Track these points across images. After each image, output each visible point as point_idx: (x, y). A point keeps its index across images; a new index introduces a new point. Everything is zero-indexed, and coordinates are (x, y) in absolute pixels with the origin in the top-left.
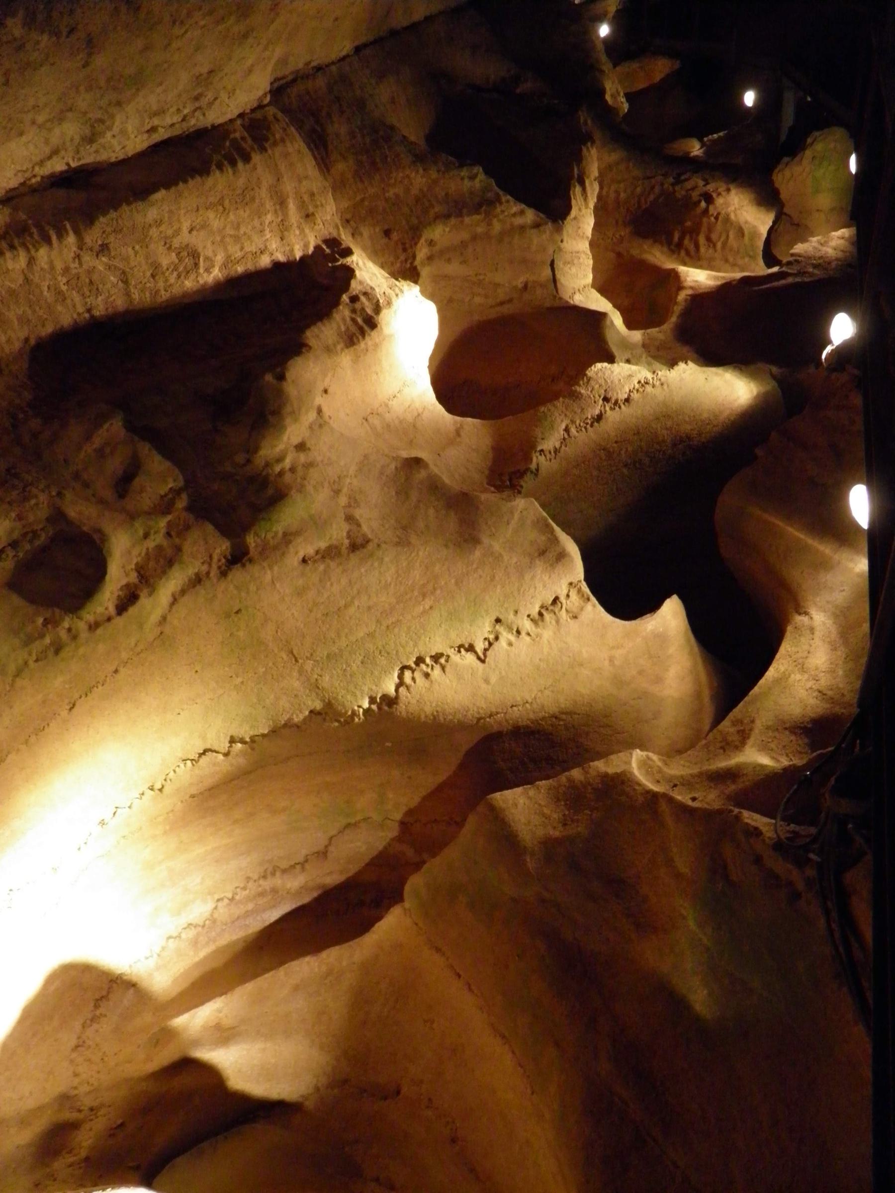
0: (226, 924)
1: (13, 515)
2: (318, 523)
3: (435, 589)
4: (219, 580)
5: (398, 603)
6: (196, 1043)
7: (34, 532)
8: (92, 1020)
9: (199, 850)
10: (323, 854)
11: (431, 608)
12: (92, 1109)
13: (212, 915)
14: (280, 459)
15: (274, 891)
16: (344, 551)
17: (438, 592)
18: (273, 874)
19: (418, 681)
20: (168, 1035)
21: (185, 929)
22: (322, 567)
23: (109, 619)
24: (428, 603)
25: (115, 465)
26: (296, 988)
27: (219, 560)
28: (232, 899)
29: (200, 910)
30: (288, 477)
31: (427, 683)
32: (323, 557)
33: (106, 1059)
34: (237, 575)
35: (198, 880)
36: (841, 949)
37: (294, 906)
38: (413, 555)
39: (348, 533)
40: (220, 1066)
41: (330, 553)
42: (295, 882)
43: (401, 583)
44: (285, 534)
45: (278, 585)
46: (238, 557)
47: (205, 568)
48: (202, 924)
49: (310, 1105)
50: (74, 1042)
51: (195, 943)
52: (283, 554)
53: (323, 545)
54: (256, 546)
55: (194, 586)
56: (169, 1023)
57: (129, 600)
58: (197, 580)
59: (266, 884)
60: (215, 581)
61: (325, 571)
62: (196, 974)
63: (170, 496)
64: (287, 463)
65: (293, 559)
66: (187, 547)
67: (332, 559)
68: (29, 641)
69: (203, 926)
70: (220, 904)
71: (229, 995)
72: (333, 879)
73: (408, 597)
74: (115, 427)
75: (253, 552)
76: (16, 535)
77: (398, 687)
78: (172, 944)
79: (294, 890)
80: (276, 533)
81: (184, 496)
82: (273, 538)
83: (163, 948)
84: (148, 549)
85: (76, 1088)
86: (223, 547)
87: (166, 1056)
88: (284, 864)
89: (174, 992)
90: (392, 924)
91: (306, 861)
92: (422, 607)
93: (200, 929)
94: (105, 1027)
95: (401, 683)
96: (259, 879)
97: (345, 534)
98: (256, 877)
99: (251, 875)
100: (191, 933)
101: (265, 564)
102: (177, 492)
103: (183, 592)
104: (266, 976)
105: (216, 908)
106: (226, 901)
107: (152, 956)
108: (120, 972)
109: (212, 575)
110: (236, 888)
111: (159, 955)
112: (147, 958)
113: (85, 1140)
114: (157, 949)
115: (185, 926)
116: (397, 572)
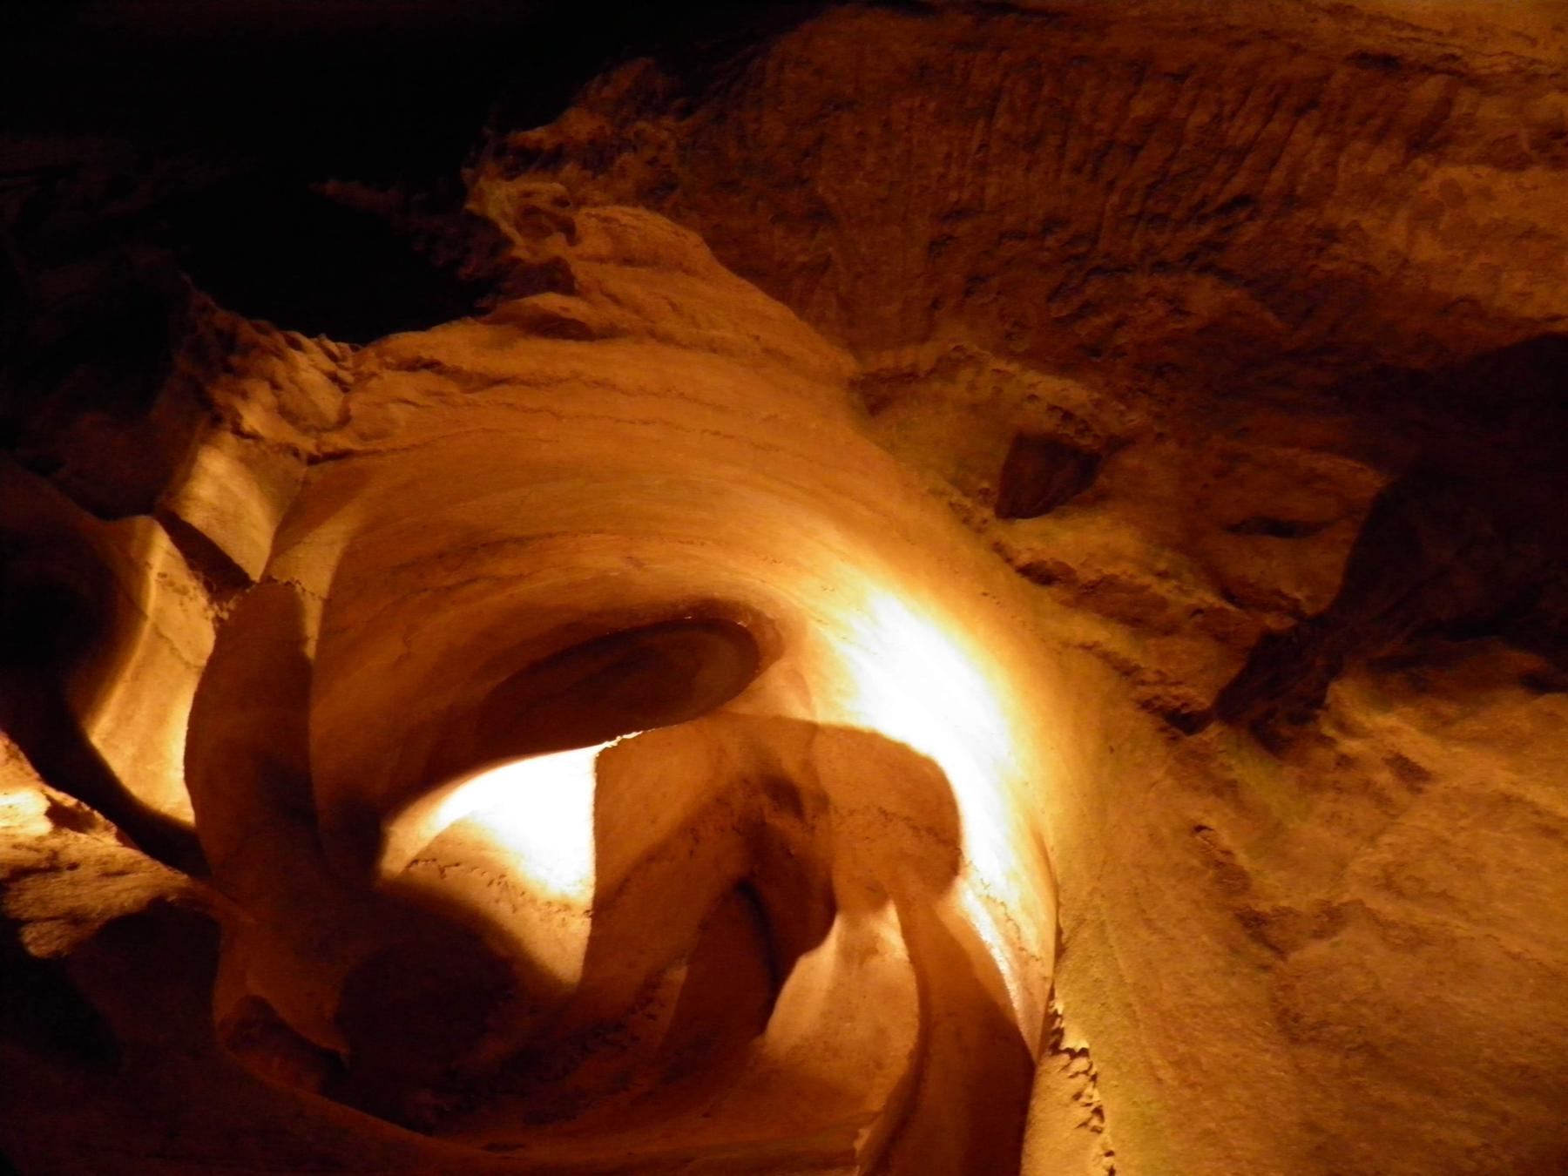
1: (1096, 396)
2: (1272, 838)
3: (1192, 1086)
4: (1138, 701)
5: (1162, 1013)
7: (1088, 429)
8: (915, 828)
11: (1159, 1081)
12: (813, 828)
14: (1346, 728)
16: (1239, 901)
17: (1187, 1093)
19: (1073, 1081)
20: (876, 899)
22: (1195, 863)
23: (1009, 560)
24: (1167, 1074)
25: (1301, 505)
27: (1177, 698)
30: (1320, 754)
31: (1067, 1098)
32: (1219, 864)
34: (1145, 725)
38: (1259, 1040)
39: (1288, 912)
41: (1228, 877)
43: (1195, 1016)
44: (1233, 785)
45: (1151, 795)
46: (1179, 722)
47: (1150, 676)
49: (757, 1041)
50: (890, 809)
52: (1197, 789)
53: (1243, 859)
54: (1206, 744)
55: (1116, 668)
57: (1041, 576)
58: (1126, 671)
60: (1133, 695)
61: (1192, 868)
63: (1284, 603)
64: (1351, 746)
65: (1198, 808)
66: (1179, 645)
67: (1218, 881)
68: (959, 483)
73: (1173, 1032)
74: (1368, 481)
75: (1193, 740)
76: (1079, 413)
77: (1070, 1051)
80: (1230, 768)
81: (1289, 622)
82: (1222, 765)
84: (1149, 586)
86: (1200, 697)
89: (946, 919)
92: (1159, 1062)
94: (908, 843)
95: (1073, 1054)
97: (1284, 903)
101: (1171, 762)
102: (1295, 609)
103: (1106, 657)
109: (1142, 689)
113: (783, 823)
116: (1215, 1007)
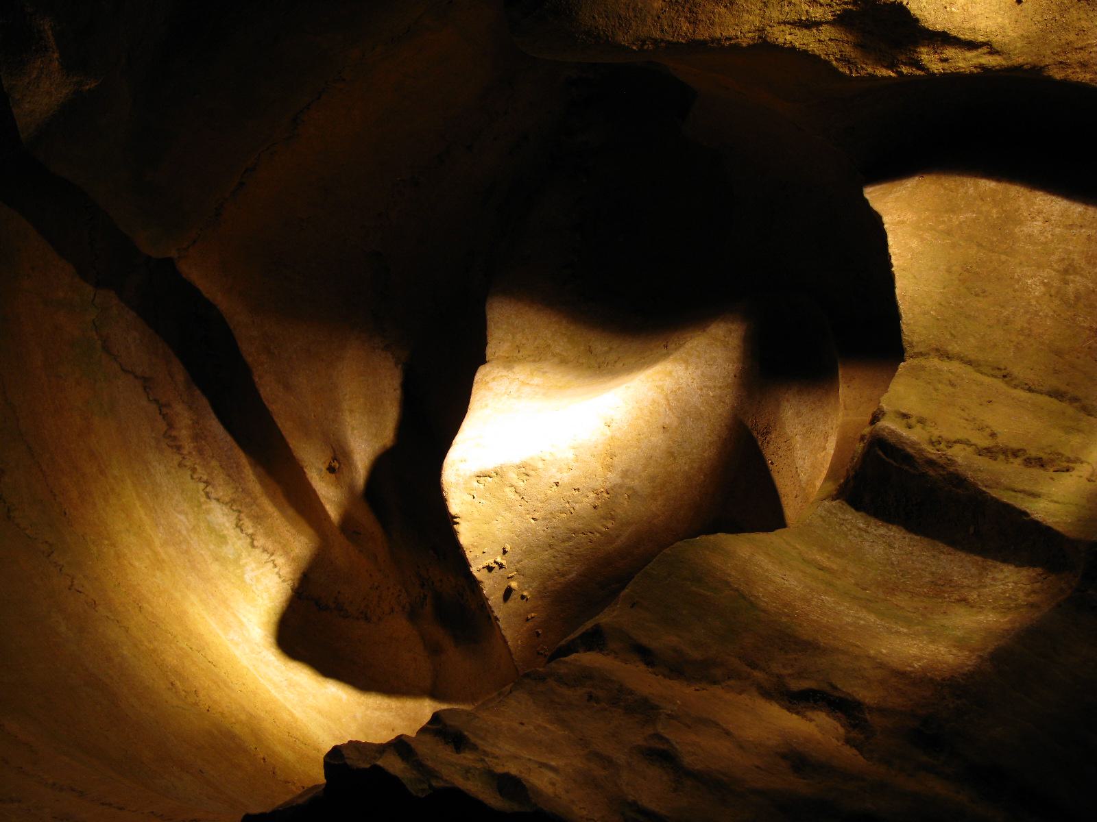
0: (237, 488)
6: (351, 488)
9: (140, 513)
10: (147, 383)
12: (423, 586)
13: (227, 504)
15: (196, 437)
18: (175, 438)
20: (348, 525)
21: (242, 530)
26: (288, 388)
28: (207, 483)
29: (221, 517)
33: (376, 584)
35: (182, 517)
36: (819, 557)
37: (213, 415)
40: (372, 458)
42: (184, 419)
48: (236, 514)
51: (257, 519)
56: (336, 525)
59: (188, 446)
62: (291, 512)
69: (240, 512)
70: (213, 495)
71: (305, 464)
72: (180, 375)
78: (260, 541)
79: (192, 415)
83: (265, 550)
85: (404, 607)
87: (367, 519)
88: (162, 426)
89: (311, 531)
90: (199, 275)
91: (156, 401)
93: (242, 515)
96: (182, 454)
98: (177, 458)
99: (176, 463)
100: (247, 523)
104: (279, 425)
105: (218, 500)
106: (209, 489)
107: (273, 561)
108: (290, 591)
110: (192, 478)
111: (272, 554)
112: (275, 566)
114: (265, 556)
115: (238, 530)
